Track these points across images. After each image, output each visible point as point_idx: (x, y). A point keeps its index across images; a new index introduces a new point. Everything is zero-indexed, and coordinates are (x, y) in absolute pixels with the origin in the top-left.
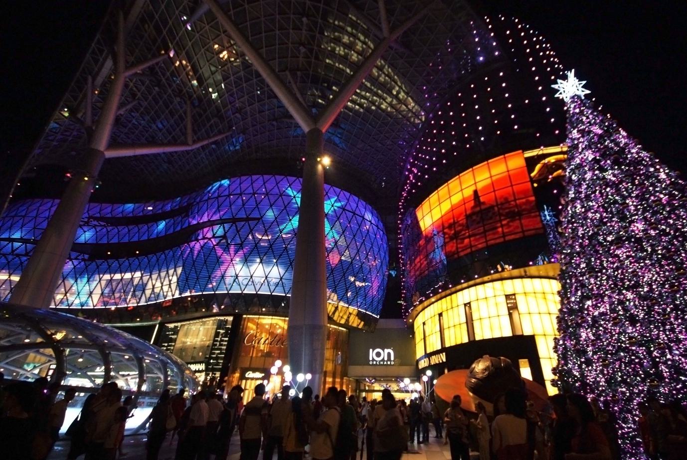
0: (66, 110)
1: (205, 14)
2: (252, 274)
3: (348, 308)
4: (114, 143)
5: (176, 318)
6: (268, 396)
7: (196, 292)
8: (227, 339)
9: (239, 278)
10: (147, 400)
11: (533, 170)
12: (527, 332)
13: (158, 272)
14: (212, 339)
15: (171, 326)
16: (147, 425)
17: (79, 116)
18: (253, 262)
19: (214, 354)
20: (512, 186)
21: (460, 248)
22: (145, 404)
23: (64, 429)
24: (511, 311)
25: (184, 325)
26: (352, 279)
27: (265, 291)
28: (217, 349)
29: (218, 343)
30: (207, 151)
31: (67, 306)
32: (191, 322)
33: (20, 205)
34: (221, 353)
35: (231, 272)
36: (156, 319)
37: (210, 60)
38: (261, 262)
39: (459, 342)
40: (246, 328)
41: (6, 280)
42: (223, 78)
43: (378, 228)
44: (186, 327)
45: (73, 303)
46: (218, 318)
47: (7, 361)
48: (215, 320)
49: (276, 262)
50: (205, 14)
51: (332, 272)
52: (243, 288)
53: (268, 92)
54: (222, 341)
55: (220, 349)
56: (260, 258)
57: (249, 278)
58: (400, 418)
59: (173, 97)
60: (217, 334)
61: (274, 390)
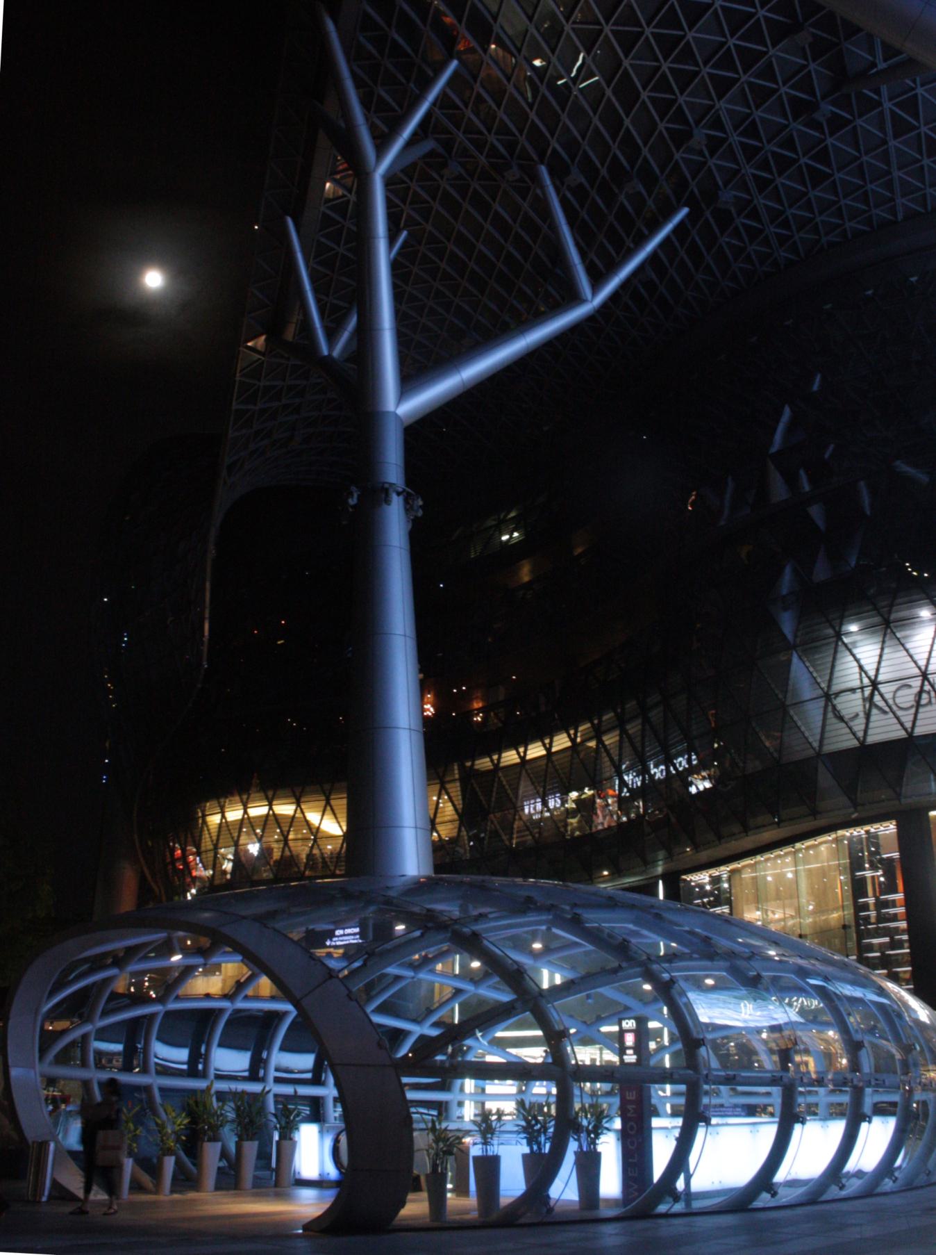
2: (922, 663)
4: (410, 379)
9: (882, 688)
10: (822, 1096)
11: (571, 72)
13: (242, 807)
14: (849, 903)
16: (276, 1137)
17: (290, 334)
18: (910, 622)
19: (870, 948)
22: (820, 1110)
28: (878, 933)
29: (873, 914)
31: (799, 850)
32: (759, 858)
34: (895, 944)
35: (848, 673)
36: (648, 863)
39: (345, 806)
46: (847, 833)
52: (907, 718)
54: (881, 905)
55: (890, 933)
57: (916, 683)
60: (858, 887)
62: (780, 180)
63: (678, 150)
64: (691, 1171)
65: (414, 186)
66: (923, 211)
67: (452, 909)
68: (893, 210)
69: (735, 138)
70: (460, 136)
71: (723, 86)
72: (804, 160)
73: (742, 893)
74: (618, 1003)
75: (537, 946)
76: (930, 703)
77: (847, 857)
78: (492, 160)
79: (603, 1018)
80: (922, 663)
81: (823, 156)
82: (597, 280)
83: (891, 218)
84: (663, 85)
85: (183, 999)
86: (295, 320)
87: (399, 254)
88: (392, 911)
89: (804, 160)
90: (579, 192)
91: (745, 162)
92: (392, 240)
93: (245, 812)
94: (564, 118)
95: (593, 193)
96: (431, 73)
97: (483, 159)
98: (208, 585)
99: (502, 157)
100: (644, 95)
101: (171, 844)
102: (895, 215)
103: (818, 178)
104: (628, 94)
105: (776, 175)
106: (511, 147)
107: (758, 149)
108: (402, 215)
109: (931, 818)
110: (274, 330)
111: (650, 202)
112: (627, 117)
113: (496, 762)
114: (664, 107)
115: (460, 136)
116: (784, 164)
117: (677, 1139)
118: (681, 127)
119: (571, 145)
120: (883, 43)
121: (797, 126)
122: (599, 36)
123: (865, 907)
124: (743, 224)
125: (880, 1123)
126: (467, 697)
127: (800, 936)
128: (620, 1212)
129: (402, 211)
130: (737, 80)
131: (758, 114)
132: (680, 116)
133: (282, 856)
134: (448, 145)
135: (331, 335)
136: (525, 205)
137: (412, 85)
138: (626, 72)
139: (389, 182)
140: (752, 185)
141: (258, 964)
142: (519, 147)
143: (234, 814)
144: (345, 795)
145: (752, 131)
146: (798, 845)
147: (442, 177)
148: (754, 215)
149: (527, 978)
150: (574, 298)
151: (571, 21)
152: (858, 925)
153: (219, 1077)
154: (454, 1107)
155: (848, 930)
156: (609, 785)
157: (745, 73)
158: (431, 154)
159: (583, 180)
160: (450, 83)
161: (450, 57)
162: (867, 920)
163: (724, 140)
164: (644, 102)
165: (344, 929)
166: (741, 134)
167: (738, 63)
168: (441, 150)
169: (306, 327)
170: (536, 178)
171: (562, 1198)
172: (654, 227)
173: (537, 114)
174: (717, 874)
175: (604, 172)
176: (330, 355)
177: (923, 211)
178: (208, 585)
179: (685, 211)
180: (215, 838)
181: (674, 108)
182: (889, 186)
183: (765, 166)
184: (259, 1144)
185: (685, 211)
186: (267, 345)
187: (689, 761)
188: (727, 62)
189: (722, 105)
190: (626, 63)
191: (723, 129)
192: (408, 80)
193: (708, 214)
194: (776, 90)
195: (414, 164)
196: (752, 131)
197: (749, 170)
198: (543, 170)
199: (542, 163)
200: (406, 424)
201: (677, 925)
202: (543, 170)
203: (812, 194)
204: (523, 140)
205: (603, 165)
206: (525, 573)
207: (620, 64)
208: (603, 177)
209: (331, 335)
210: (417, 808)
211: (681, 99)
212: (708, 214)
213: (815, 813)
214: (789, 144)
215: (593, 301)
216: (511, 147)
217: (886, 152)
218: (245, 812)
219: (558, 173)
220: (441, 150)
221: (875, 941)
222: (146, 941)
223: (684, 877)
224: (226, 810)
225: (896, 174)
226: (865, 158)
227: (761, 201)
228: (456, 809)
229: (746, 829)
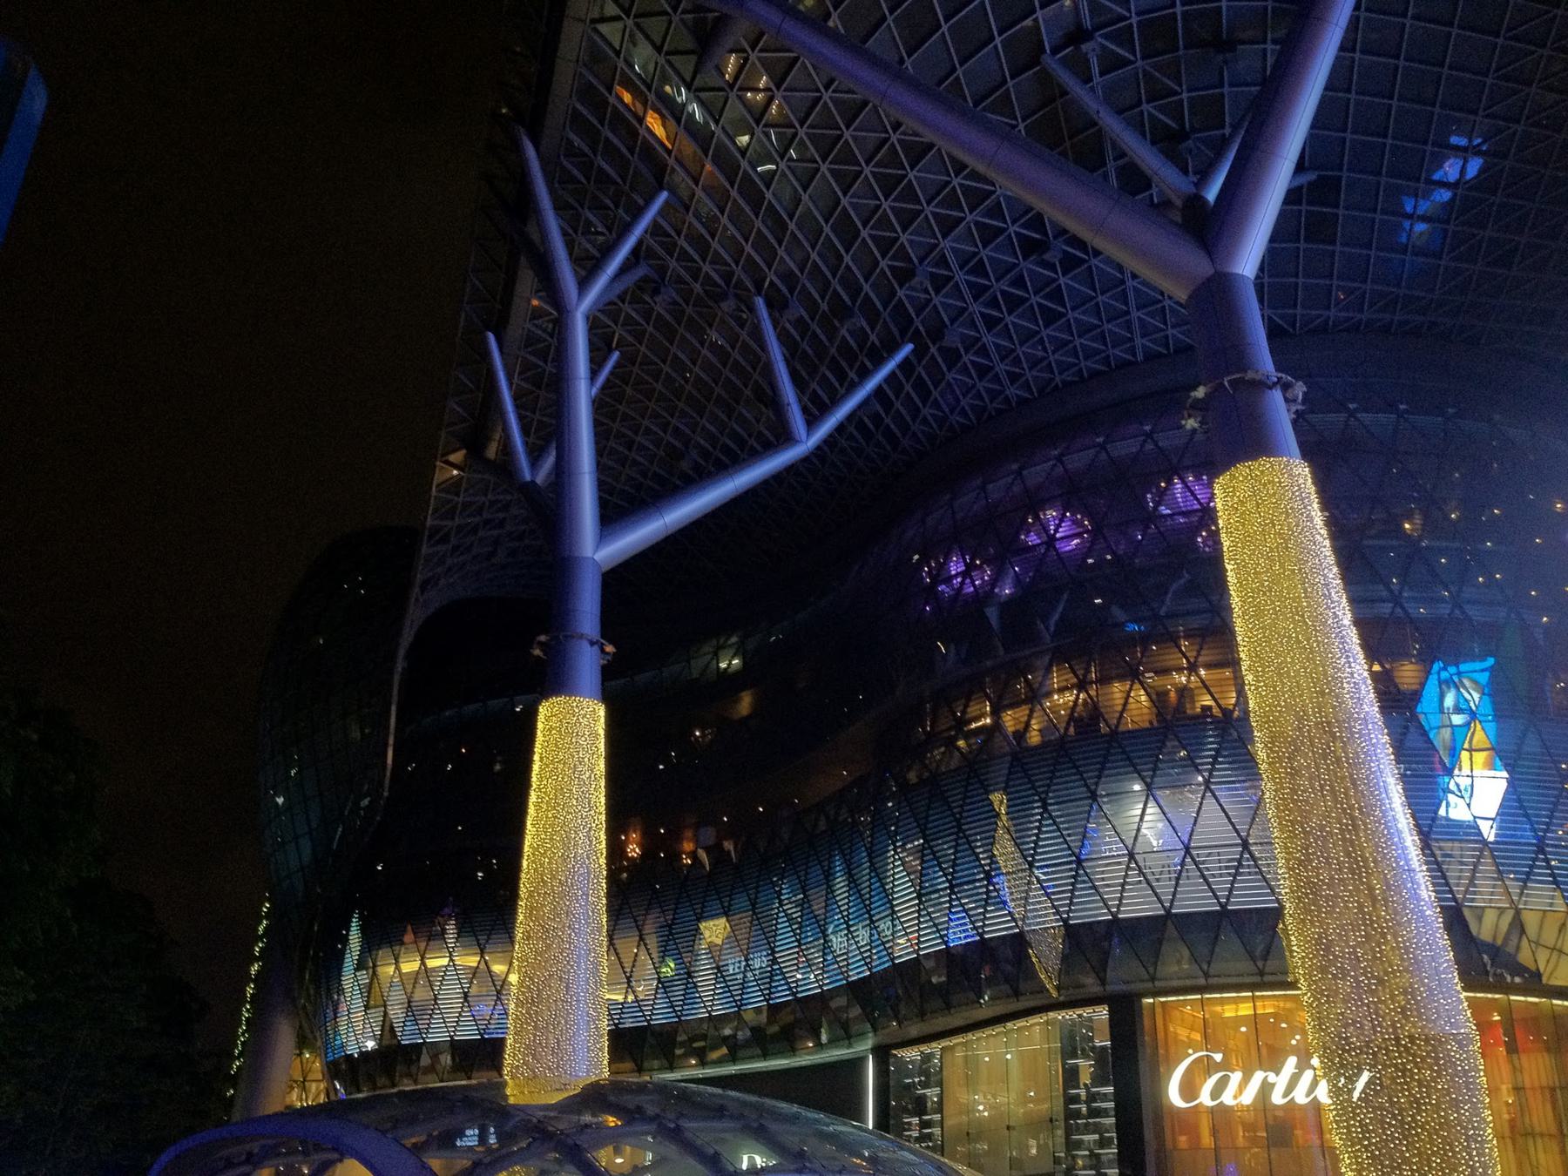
1: (972, 170)
4: (613, 515)
5: (914, 1031)
8: (1111, 1089)
13: (418, 958)
15: (911, 1054)
17: (492, 451)
24: (1407, 673)
25: (951, 1048)
27: (1195, 900)
28: (1087, 1129)
34: (1103, 1143)
37: (693, 78)
38: (1149, 788)
41: (418, 973)
44: (959, 1054)
48: (1047, 1023)
49: (1207, 783)
50: (972, 170)
51: (499, 999)
54: (1092, 1098)
55: (1097, 1129)
56: (1143, 779)
59: (711, 304)
60: (1071, 1076)
62: (1009, 319)
63: (901, 288)
65: (626, 307)
66: (1166, 352)
68: (1133, 352)
69: (960, 276)
70: (673, 264)
71: (948, 226)
72: (1035, 299)
73: (953, 1074)
77: (1058, 1041)
78: (708, 288)
80: (1130, 842)
81: (1056, 296)
82: (812, 422)
83: (1131, 358)
84: (884, 223)
86: (497, 438)
87: (604, 388)
89: (1035, 299)
90: (800, 323)
92: (594, 374)
93: (423, 963)
94: (781, 252)
95: (814, 326)
96: (641, 202)
97: (697, 287)
98: (394, 708)
99: (719, 286)
100: (864, 233)
101: (336, 997)
102: (1134, 355)
103: (1051, 318)
104: (848, 233)
105: (1006, 314)
106: (728, 276)
107: (987, 288)
108: (613, 337)
109: (1144, 1006)
110: (474, 443)
111: (873, 337)
112: (847, 253)
114: (886, 245)
115: (673, 264)
116: (1014, 303)
118: (902, 265)
119: (788, 277)
121: (1028, 266)
122: (816, 174)
123: (1075, 1099)
124: (973, 362)
126: (675, 836)
127: (1008, 1128)
129: (614, 333)
130: (963, 219)
131: (985, 253)
132: (902, 254)
134: (662, 270)
135: (535, 462)
136: (744, 333)
137: (621, 211)
138: (844, 209)
139: (593, 324)
140: (980, 323)
142: (736, 277)
143: (410, 966)
145: (979, 270)
146: (1009, 1025)
147: (656, 303)
148: (983, 352)
149: (724, 1160)
150: (784, 437)
151: (786, 159)
152: (1067, 1119)
157: (971, 213)
158: (645, 279)
159: (804, 313)
160: (661, 213)
161: (661, 188)
162: (1077, 1114)
163: (950, 278)
164: (864, 239)
166: (968, 273)
167: (964, 205)
168: (656, 277)
169: (507, 448)
170: (752, 309)
172: (879, 362)
175: (824, 306)
176: (533, 482)
177: (1166, 352)
178: (394, 708)
179: (909, 347)
182: (1128, 326)
183: (994, 303)
185: (909, 347)
186: (465, 461)
188: (953, 203)
189: (946, 244)
190: (844, 201)
191: (948, 268)
192: (617, 207)
193: (933, 350)
194: (1005, 230)
195: (625, 292)
196: (979, 270)
197: (976, 308)
198: (760, 302)
199: (760, 295)
200: (605, 568)
202: (760, 302)
203: (1044, 333)
204: (738, 271)
205: (823, 298)
206: (745, 704)
207: (838, 202)
208: (824, 311)
209: (535, 462)
211: (904, 238)
212: (933, 350)
213: (1017, 994)
214: (1019, 282)
215: (807, 441)
216: (728, 276)
217: (1124, 293)
218: (423, 963)
219: (777, 305)
220: (656, 277)
221: (1086, 1138)
223: (894, 1052)
224: (401, 960)
225: (1135, 314)
226: (1100, 298)
227: (988, 339)
229: (948, 1006)
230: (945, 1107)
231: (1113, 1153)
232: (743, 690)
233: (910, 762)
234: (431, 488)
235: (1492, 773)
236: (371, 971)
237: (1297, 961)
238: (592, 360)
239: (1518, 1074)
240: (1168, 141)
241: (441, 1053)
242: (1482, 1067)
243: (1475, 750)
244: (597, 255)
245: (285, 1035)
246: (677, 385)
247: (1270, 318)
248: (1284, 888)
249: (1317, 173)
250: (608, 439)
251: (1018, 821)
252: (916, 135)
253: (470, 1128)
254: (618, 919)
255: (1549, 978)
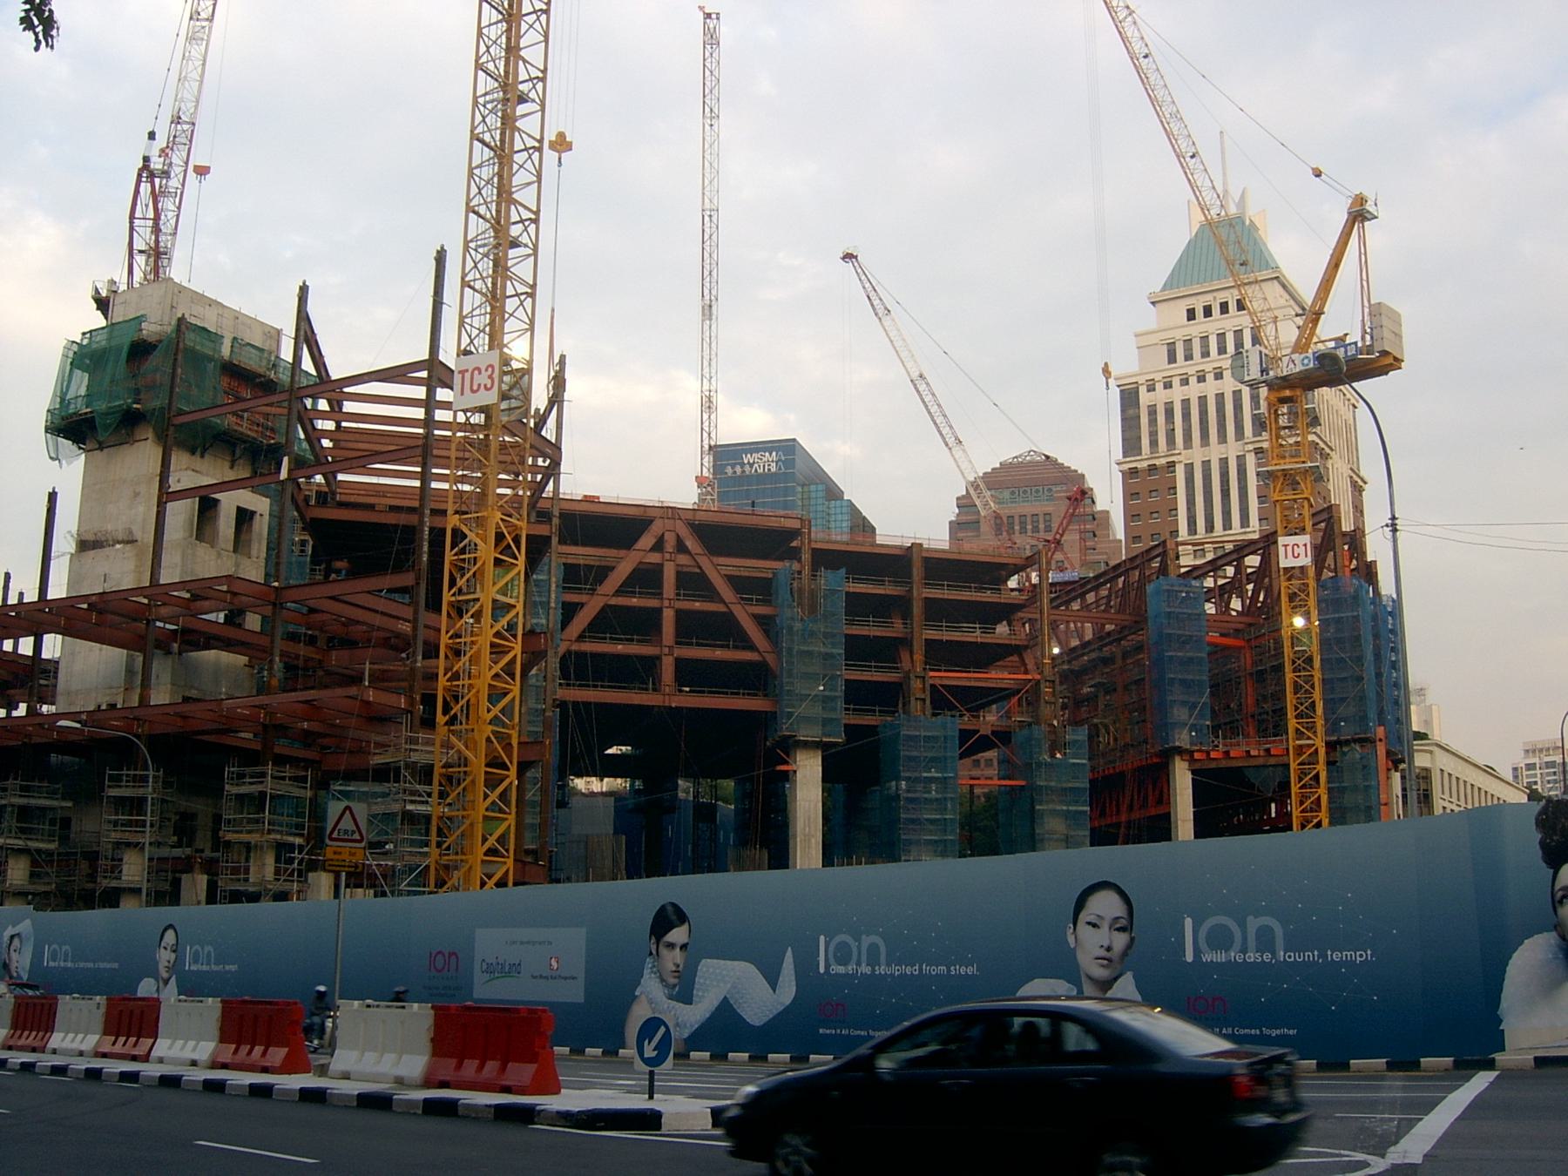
0: (1234, 613)
3: (167, 880)
6: (476, 1062)
7: (937, 772)
12: (121, 904)
20: (531, 26)
21: (418, 382)
23: (789, 953)
24: (156, 996)
26: (478, 490)
30: (1269, 718)
33: (205, 738)
40: (215, 456)
42: (1286, 1087)
43: (476, 267)
45: (97, 289)
47: (508, 764)
53: (1310, 746)
58: (379, 739)
61: (97, 291)
64: (522, 32)
67: (1281, 1051)
74: (507, 584)
75: (1194, 734)
76: (84, 334)
79: (394, 1112)
85: (465, 1117)
88: (1104, 583)
91: (569, 561)
113: (1091, 1045)
117: (639, 984)
120: (582, 605)
125: (427, 1027)
128: (1243, 1118)
133: (86, 1035)
141: (1085, 645)
144: (53, 594)
153: (1425, 1071)
154: (791, 774)
155: (682, 1050)
156: (1341, 353)
165: (164, 628)
171: (444, 306)
173: (605, 609)
174: (254, 552)
180: (341, 597)
181: (634, 601)
184: (28, 707)
187: (315, 404)
201: (649, 1043)
210: (609, 507)
222: (399, 504)
228: (1238, 1075)
230: (92, 553)
231: (645, 1085)
232: (6, 638)
233: (393, 640)
234: (1330, 801)
235: (64, 544)
236: (181, 345)
237: (577, 692)
238: (948, 686)
239: (957, 452)
240: (424, 886)
241: (1009, 625)
242: (839, 1031)
243: (522, 150)
244: (544, 7)
245: (542, 412)
246: (1396, 693)
247: (650, 522)
248: (966, 773)
249: (1123, 538)
250: (1345, 788)
251: (1161, 418)
252: (1256, 1055)
253: (338, 560)
254: (314, 527)
255: (194, 503)
